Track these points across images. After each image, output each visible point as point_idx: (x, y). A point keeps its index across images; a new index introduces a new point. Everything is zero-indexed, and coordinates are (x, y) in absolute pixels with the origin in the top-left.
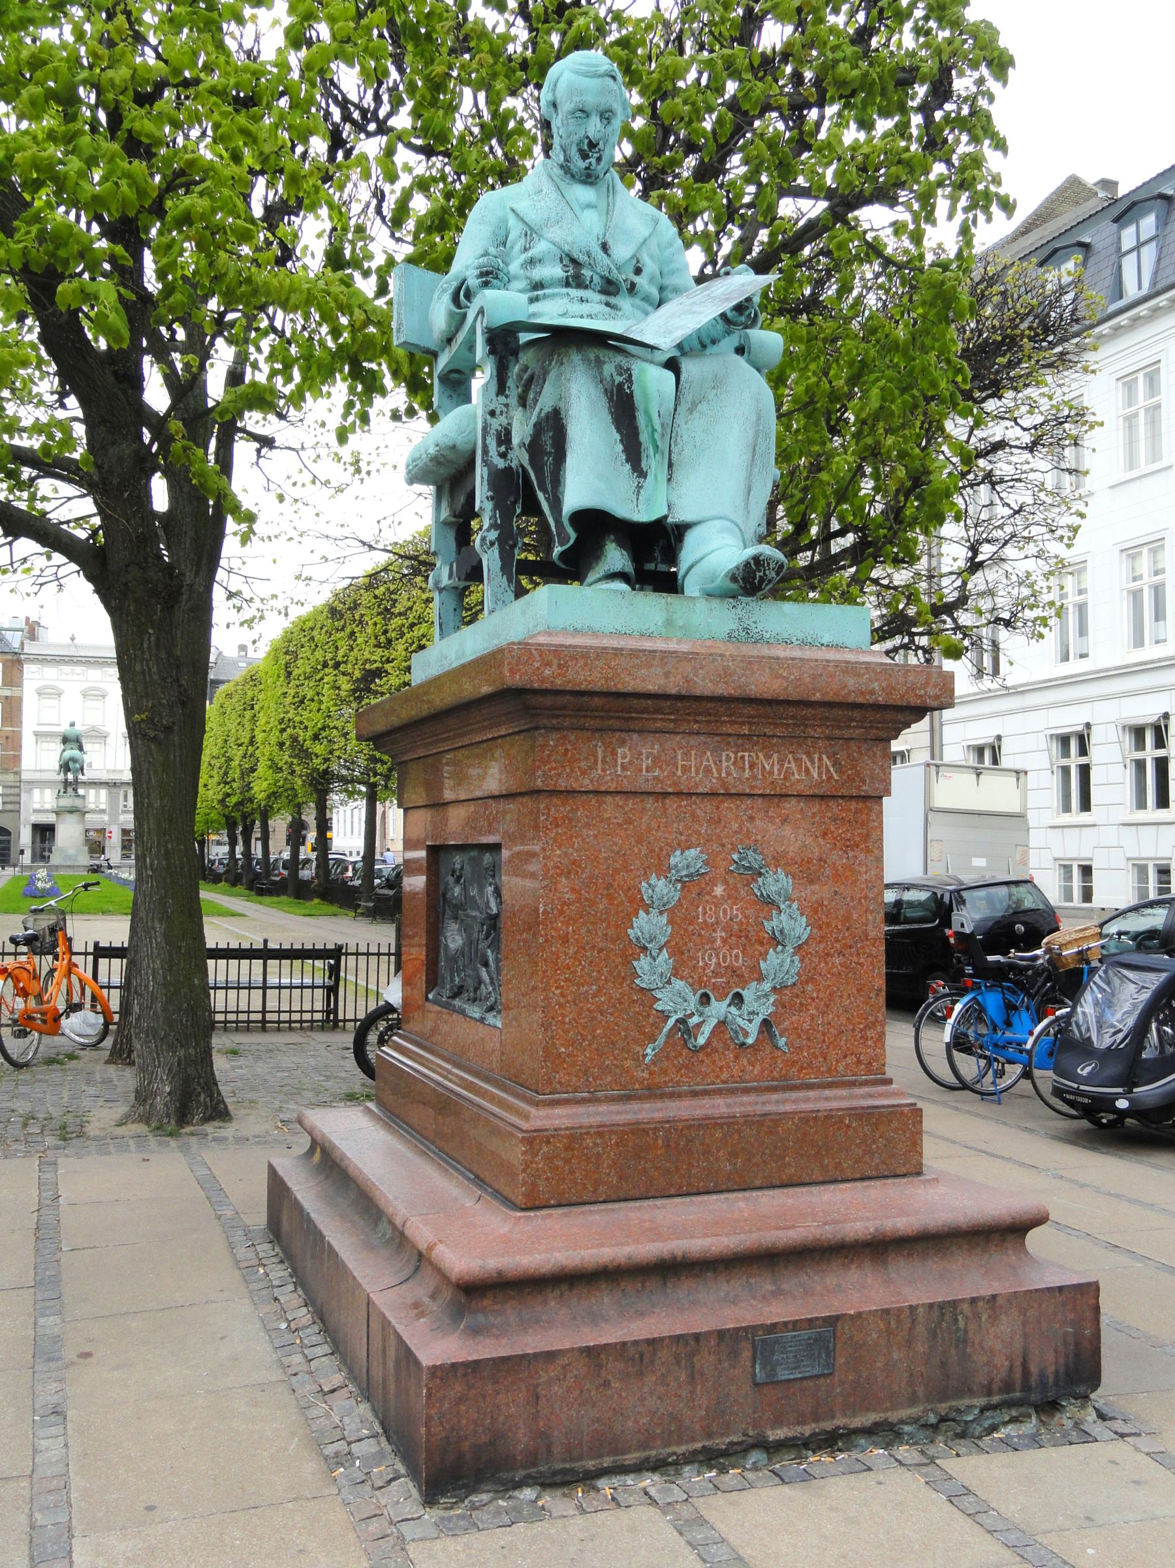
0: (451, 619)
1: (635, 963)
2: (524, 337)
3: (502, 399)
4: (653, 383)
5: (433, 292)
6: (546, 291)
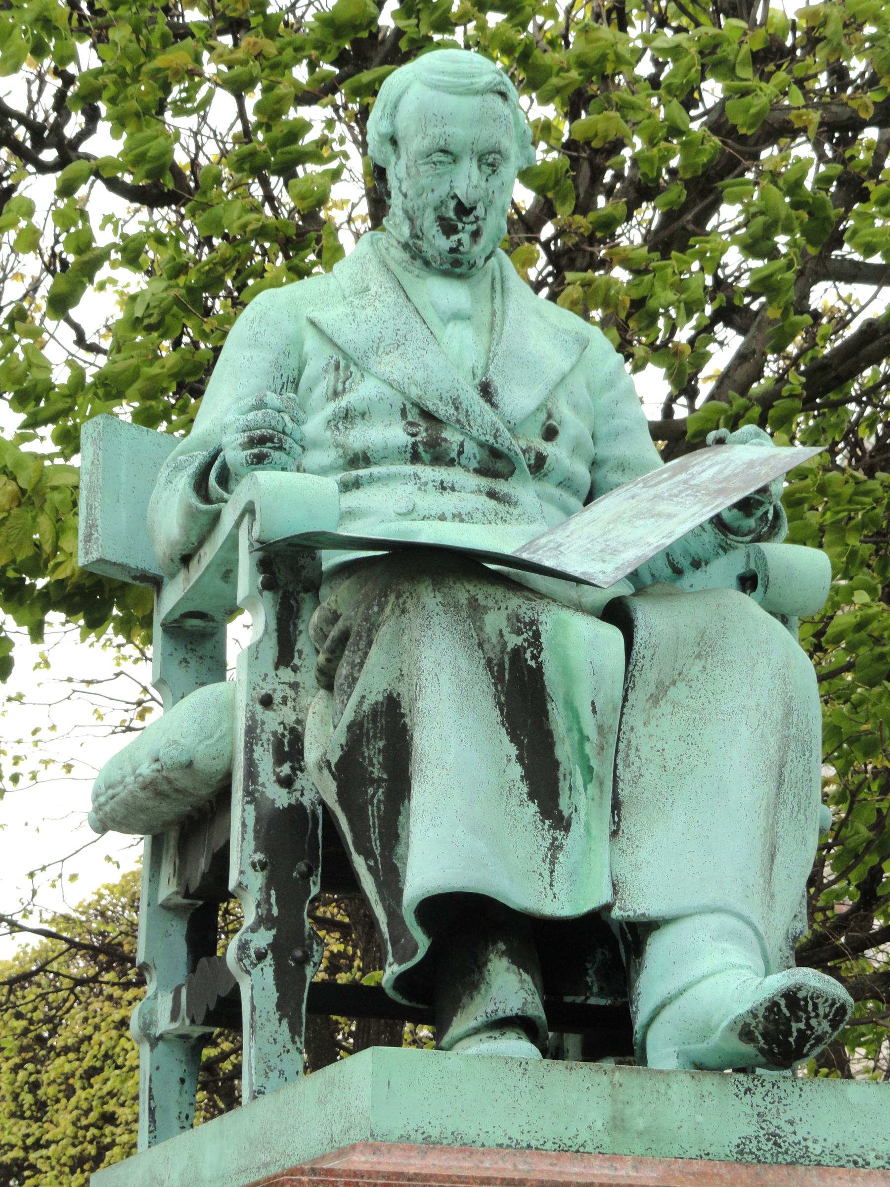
0: (172, 1100)
2: (331, 559)
3: (286, 674)
4: (580, 650)
5: (157, 466)
6: (375, 470)
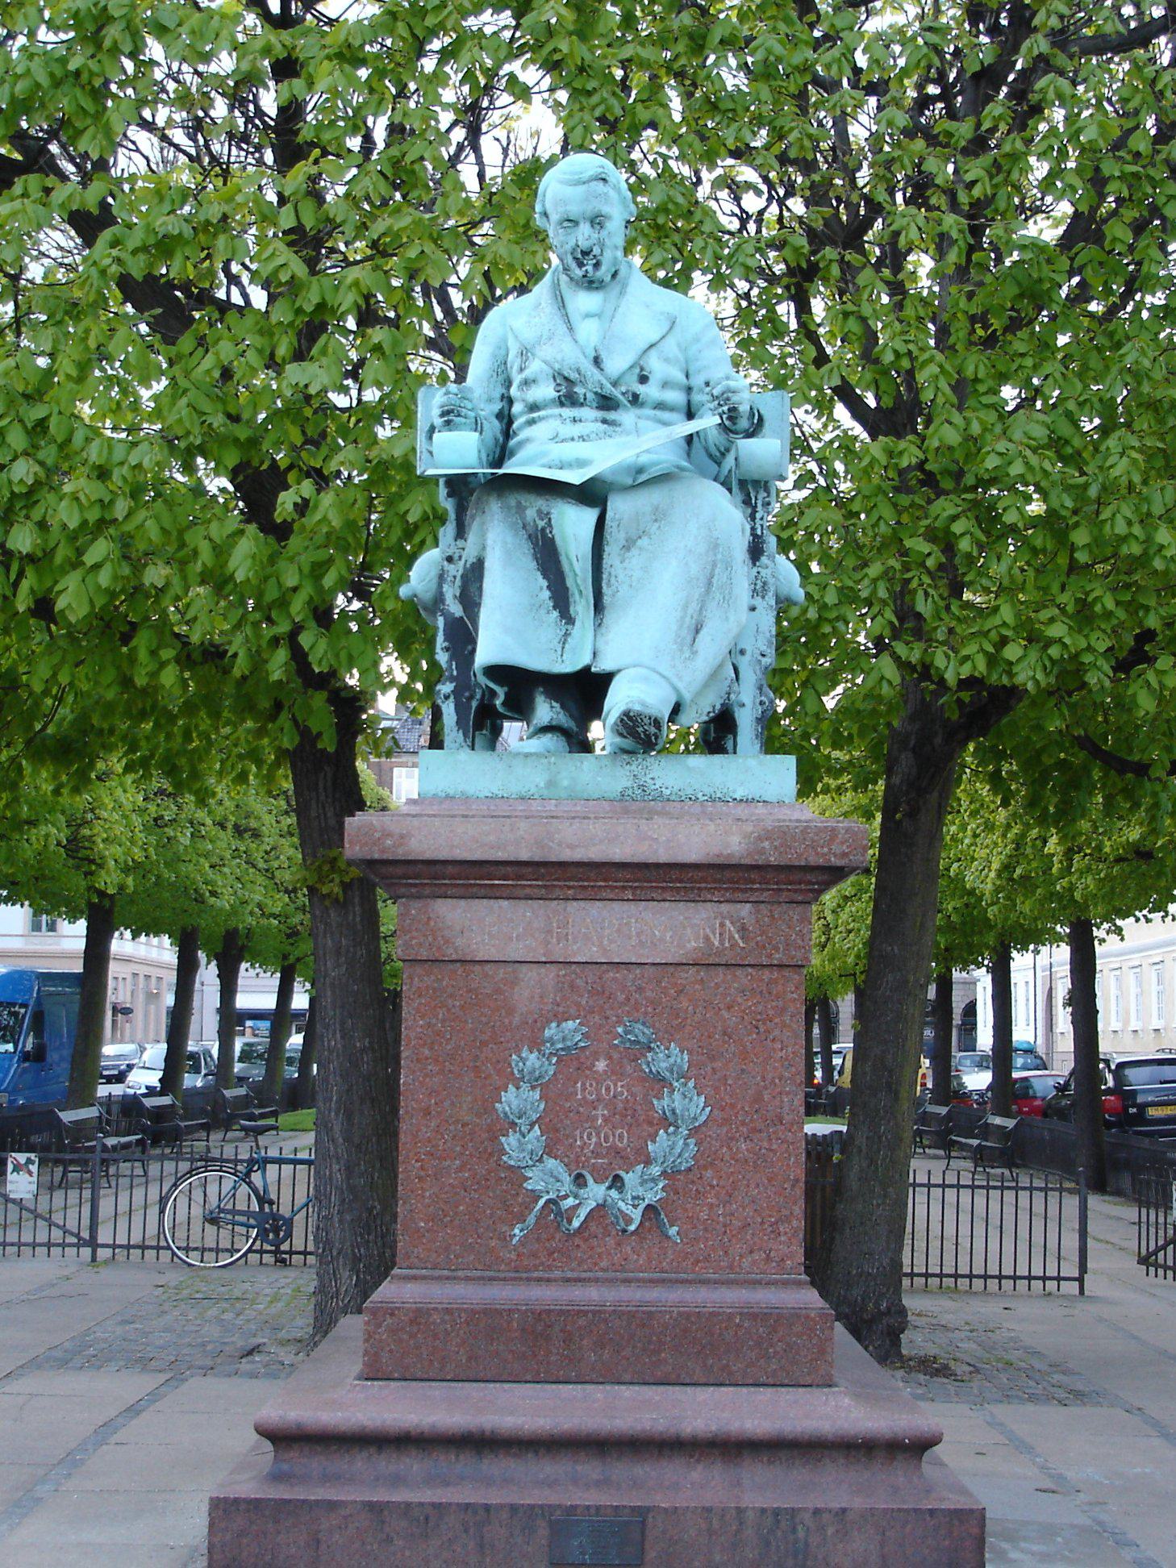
1: (503, 1139)
4: (573, 525)
6: (542, 413)
